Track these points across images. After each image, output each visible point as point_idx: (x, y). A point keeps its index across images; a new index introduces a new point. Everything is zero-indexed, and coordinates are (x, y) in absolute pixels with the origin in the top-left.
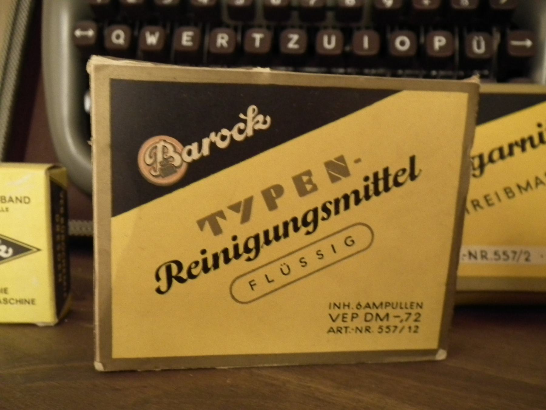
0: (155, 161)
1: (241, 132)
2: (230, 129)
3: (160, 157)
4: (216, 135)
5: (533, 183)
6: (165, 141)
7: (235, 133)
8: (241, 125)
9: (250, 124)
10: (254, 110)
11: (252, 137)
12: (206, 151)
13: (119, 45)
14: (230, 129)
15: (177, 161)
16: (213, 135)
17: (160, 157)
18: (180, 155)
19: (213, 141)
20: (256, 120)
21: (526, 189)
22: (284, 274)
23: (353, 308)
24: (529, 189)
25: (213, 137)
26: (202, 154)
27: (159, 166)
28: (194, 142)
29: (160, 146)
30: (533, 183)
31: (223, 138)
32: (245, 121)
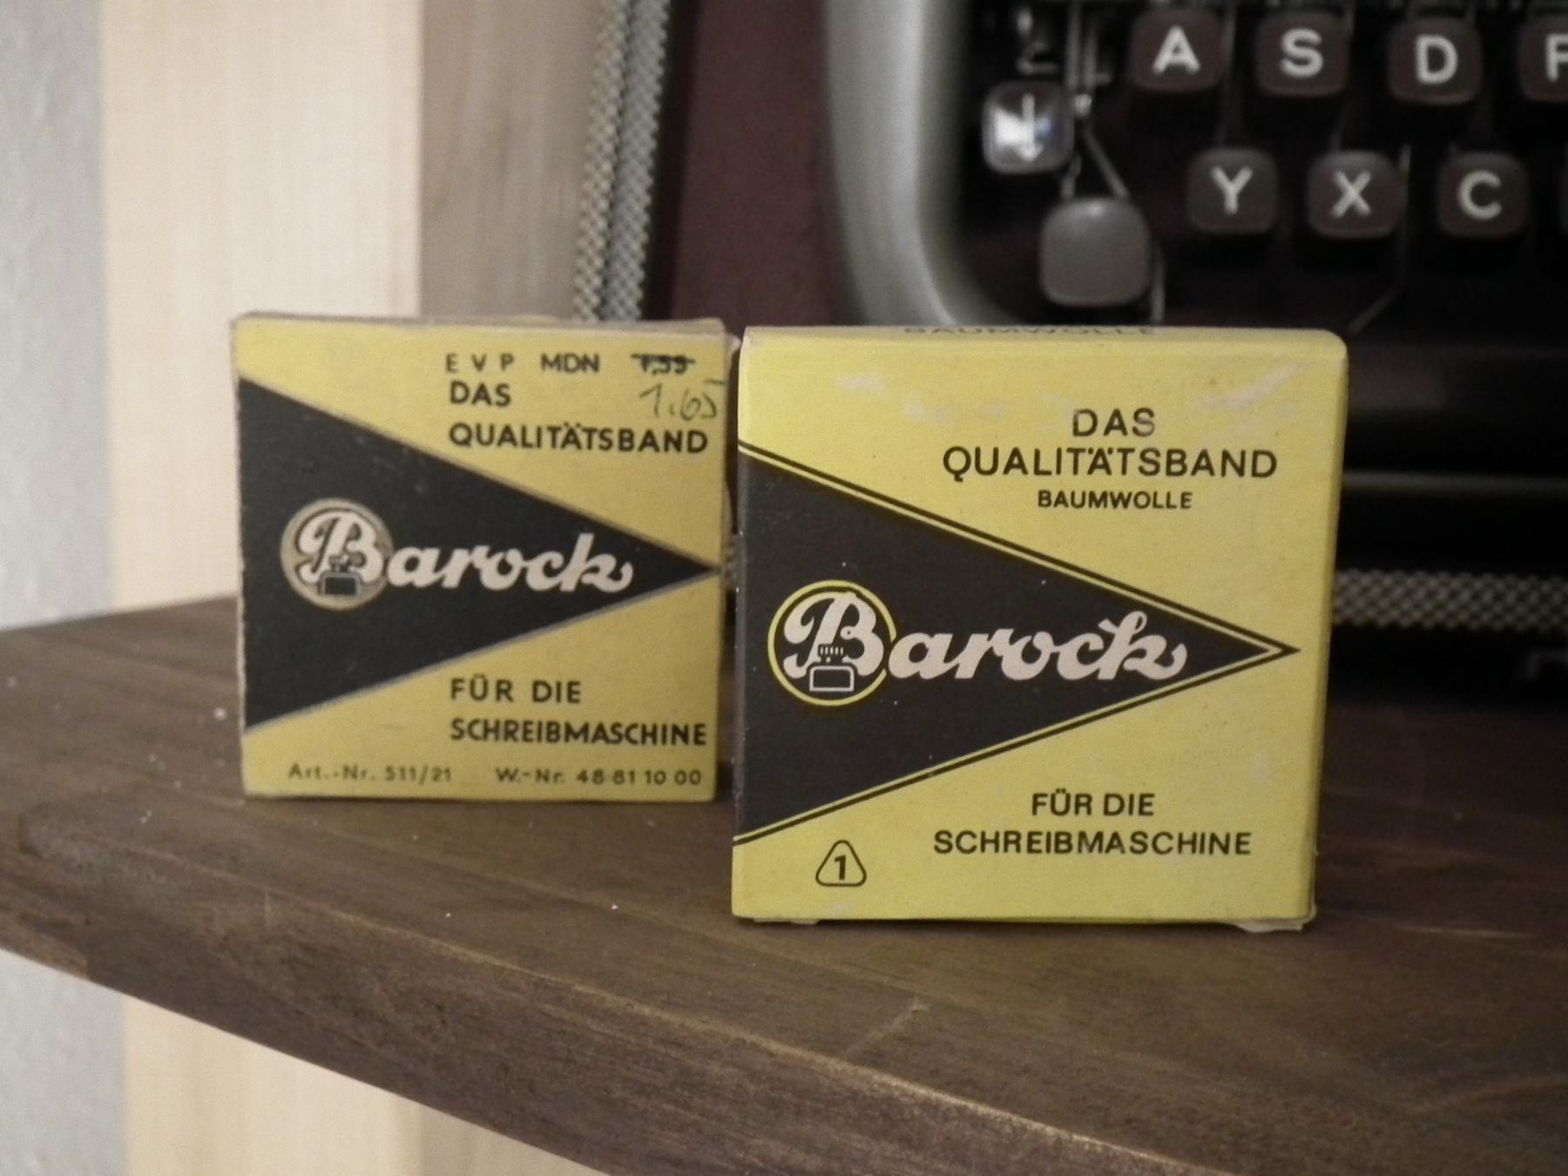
0: (322, 550)
1: (1086, 656)
2: (529, 555)
3: (334, 547)
4: (490, 555)
5: (592, 731)
6: (859, 595)
7: (535, 567)
8: (556, 558)
9: (1120, 647)
10: (1140, 621)
11: (567, 595)
12: (967, 665)
13: (1432, 32)
14: (529, 555)
15: (369, 573)
16: (1003, 635)
17: (826, 635)
18: (888, 647)
19: (998, 652)
20: (1139, 644)
21: (576, 736)
22: (847, 843)
23: (373, 778)
24: (581, 738)
25: (482, 559)
26: (441, 580)
27: (325, 566)
28: (431, 545)
29: (842, 602)
30: (592, 731)
31: (504, 568)
32: (1108, 639)
